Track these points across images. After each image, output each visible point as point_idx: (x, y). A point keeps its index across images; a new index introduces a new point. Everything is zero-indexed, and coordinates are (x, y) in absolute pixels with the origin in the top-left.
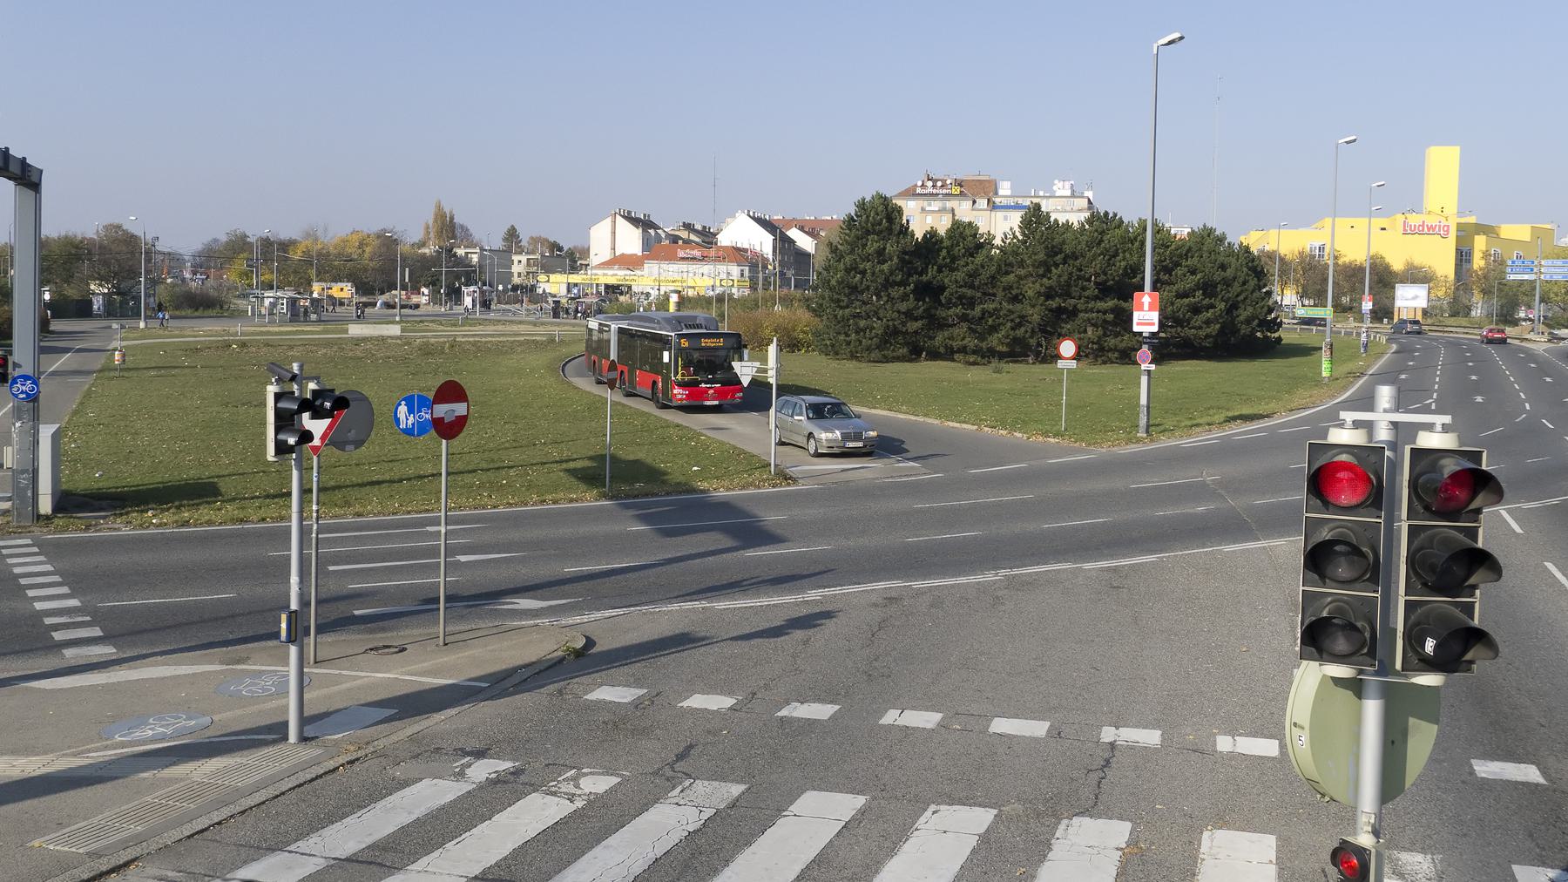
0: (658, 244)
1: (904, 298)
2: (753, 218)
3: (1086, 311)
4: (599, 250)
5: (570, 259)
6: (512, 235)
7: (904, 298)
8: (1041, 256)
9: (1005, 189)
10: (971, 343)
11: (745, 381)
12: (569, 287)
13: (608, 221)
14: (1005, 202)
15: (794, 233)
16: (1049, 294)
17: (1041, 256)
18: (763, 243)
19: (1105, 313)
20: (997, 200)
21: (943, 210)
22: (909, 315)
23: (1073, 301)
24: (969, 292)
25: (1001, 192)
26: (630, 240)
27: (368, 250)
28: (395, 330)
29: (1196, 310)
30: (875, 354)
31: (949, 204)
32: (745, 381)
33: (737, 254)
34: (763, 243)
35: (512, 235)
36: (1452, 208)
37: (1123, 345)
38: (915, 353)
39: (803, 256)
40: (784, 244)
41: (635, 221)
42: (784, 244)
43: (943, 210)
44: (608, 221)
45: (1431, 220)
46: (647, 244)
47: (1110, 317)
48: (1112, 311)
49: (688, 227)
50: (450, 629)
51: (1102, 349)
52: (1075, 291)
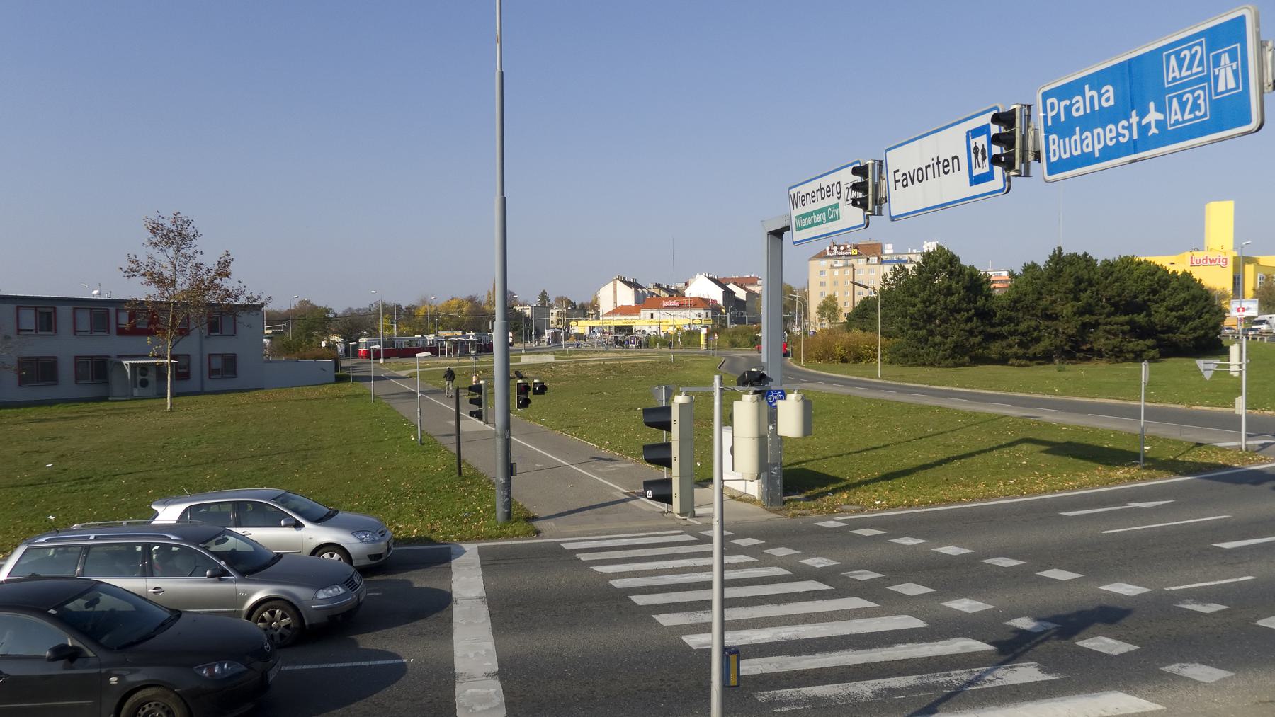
0: (645, 300)
1: (969, 320)
2: (712, 279)
3: (1106, 324)
4: (606, 305)
5: (586, 310)
6: (544, 296)
7: (969, 320)
8: (1071, 285)
9: (889, 249)
10: (1021, 352)
11: (1208, 375)
12: (592, 328)
13: (612, 284)
14: (889, 258)
15: (731, 287)
16: (1081, 312)
17: (1071, 285)
18: (717, 294)
19: (1122, 325)
20: (884, 257)
21: (846, 266)
22: (971, 332)
23: (1095, 317)
24: (1014, 314)
25: (886, 252)
26: (627, 297)
27: (464, 309)
28: (550, 358)
29: (1184, 320)
30: (950, 361)
31: (850, 262)
32: (1208, 375)
33: (702, 302)
34: (717, 294)
35: (544, 296)
36: (1229, 243)
37: (1139, 348)
38: (978, 360)
39: (739, 301)
40: (728, 294)
41: (629, 284)
42: (728, 294)
43: (846, 266)
44: (612, 284)
45: (1211, 257)
46: (638, 298)
47: (1127, 328)
48: (1128, 323)
49: (659, 286)
50: (727, 560)
51: (1121, 351)
52: (1097, 310)
